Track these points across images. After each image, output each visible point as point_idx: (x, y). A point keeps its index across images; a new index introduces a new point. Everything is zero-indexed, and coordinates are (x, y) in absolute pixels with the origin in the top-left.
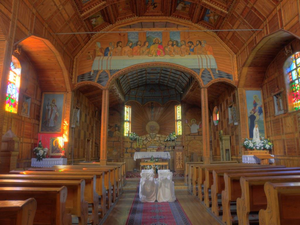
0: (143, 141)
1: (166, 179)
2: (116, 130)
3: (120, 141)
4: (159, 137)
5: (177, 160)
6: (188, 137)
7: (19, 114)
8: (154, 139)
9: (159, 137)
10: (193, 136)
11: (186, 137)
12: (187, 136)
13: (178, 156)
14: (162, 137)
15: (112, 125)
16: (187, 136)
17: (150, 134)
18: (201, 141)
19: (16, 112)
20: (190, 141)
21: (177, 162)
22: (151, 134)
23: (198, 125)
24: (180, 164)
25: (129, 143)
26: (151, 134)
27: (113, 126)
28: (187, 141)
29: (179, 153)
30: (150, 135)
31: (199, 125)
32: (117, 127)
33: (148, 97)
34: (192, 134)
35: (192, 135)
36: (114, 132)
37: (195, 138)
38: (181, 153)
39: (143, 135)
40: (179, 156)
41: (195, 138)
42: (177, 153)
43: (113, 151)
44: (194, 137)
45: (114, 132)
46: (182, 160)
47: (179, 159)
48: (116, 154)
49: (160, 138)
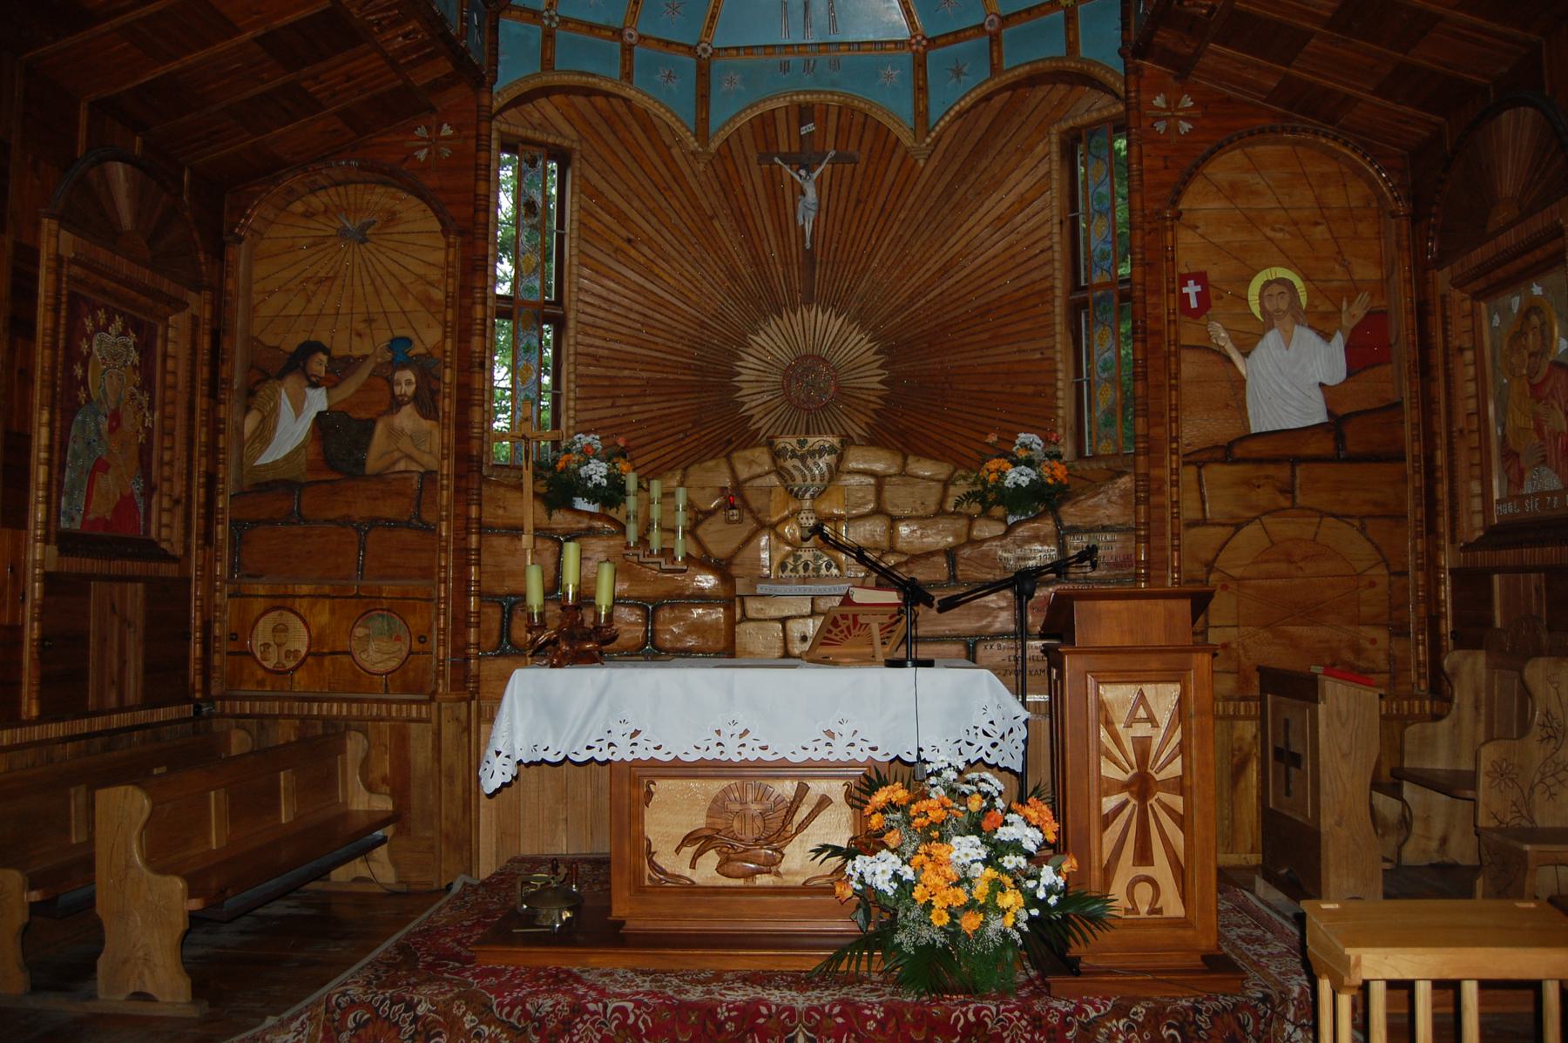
0: (698, 517)
1: (604, 863)
2: (396, 404)
3: (428, 517)
4: (880, 479)
5: (1109, 803)
6: (1218, 473)
7: (482, 640)
8: (817, 496)
9: (880, 479)
10: (1270, 470)
11: (1189, 474)
12: (1200, 465)
13: (1126, 736)
14: (903, 473)
15: (360, 348)
16: (1200, 465)
17: (770, 444)
18: (1362, 530)
19: (390, 807)
20: (1238, 527)
21: (1107, 821)
22: (788, 442)
23: (1327, 336)
24: (1144, 855)
25: (527, 540)
26: (788, 442)
27: (365, 357)
28: (1203, 522)
29: (1141, 693)
30: (777, 455)
31: (1339, 341)
32: (842, 443)
33: (678, 120)
34: (1255, 447)
35: (1259, 461)
36: (374, 422)
37: (1288, 490)
38: (1164, 698)
39: (700, 461)
40: (1142, 745)
41: (1288, 490)
42: (1117, 695)
43: (360, 632)
44: (1283, 473)
45: (380, 428)
46: (1178, 802)
47: (1142, 786)
48: (394, 664)
49: (888, 493)
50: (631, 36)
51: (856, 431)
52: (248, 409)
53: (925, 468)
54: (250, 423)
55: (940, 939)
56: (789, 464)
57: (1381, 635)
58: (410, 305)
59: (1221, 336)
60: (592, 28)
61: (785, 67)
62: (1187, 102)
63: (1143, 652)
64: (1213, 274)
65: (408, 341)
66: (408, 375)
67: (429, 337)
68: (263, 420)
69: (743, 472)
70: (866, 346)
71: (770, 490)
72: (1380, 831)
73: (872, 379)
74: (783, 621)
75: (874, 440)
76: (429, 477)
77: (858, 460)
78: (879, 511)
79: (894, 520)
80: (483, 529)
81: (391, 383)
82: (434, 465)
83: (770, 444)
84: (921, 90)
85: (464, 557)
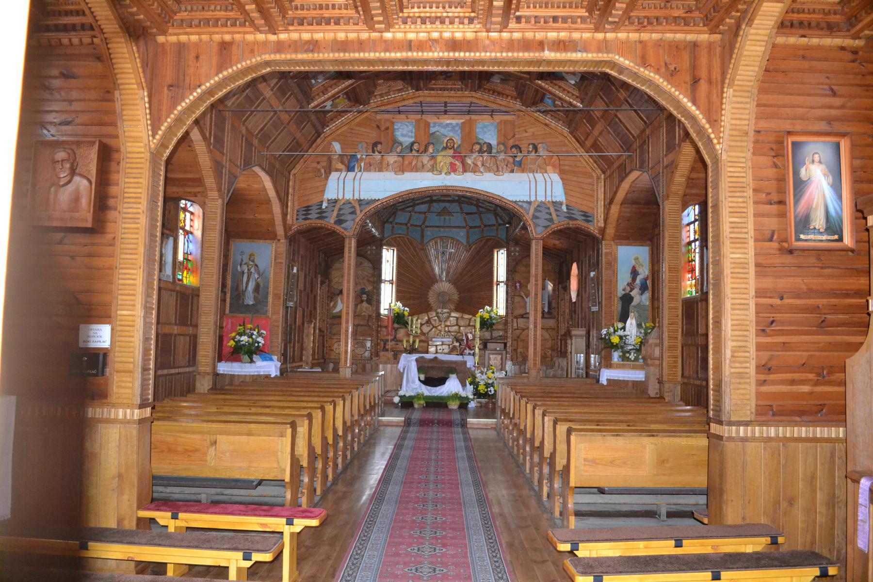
4: (457, 318)
8: (445, 321)
9: (457, 318)
12: (517, 318)
14: (462, 317)
16: (517, 318)
22: (439, 311)
26: (439, 311)
30: (437, 313)
50: (409, 225)
51: (453, 307)
52: (331, 301)
53: (466, 316)
54: (332, 304)
55: (596, 232)
56: (440, 315)
57: (550, 351)
58: (365, 281)
59: (522, 294)
60: (401, 224)
61: (440, 231)
62: (518, 249)
63: (231, 503)
64: (522, 282)
65: (364, 289)
66: (365, 296)
67: (369, 288)
68: (334, 304)
69: (430, 316)
70: (449, 285)
71: (435, 320)
72: (706, 521)
73: (456, 297)
74: (436, 346)
75: (457, 310)
76: (370, 316)
77: (453, 314)
78: (457, 325)
79: (460, 327)
80: (381, 327)
81: (361, 297)
82: (370, 314)
83: (436, 311)
84: (468, 237)
85: (378, 332)
